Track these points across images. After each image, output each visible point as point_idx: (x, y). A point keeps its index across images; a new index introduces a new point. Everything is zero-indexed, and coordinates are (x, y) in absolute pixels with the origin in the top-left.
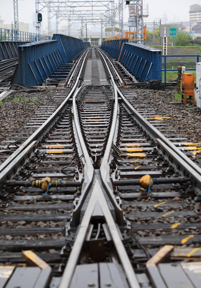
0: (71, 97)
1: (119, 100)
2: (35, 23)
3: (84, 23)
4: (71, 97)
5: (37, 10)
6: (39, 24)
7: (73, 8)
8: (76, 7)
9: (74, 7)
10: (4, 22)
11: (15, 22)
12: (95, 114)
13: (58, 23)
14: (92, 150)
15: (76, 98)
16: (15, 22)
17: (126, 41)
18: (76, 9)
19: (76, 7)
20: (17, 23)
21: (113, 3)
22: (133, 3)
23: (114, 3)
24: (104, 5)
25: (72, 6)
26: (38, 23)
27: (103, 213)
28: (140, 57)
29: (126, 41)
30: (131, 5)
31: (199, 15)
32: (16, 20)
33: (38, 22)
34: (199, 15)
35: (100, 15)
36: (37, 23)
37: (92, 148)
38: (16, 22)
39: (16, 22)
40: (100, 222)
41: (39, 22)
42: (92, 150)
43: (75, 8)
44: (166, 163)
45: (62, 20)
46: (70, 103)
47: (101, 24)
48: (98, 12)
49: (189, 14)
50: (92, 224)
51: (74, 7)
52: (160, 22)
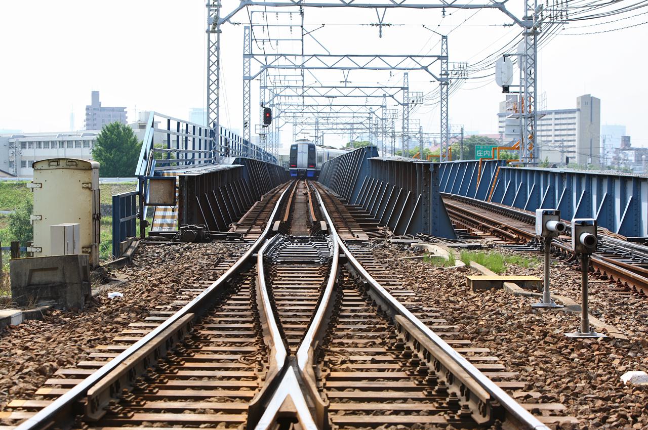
0: (256, 250)
1: (340, 259)
2: (258, 127)
3: (320, 130)
4: (256, 250)
5: (263, 102)
6: (264, 130)
7: (331, 99)
8: (336, 97)
9: (333, 97)
10: (159, 124)
11: (245, 124)
12: (289, 273)
13: (279, 128)
14: (285, 326)
15: (264, 253)
16: (245, 124)
17: (503, 164)
18: (335, 101)
19: (336, 97)
20: (248, 125)
21: (406, 91)
22: (519, 91)
23: (408, 92)
24: (390, 96)
25: (329, 94)
26: (263, 126)
27: (295, 408)
28: (406, 191)
29: (503, 164)
30: (511, 94)
31: (556, 119)
32: (247, 119)
33: (263, 124)
34: (556, 119)
35: (368, 115)
36: (261, 127)
37: (285, 323)
38: (247, 123)
39: (247, 123)
40: (293, 422)
41: (266, 125)
42: (285, 326)
43: (335, 99)
44: (400, 343)
45: (286, 123)
46: (252, 260)
47: (316, 130)
48: (346, 109)
49: (497, 119)
50: (278, 423)
51: (333, 97)
52: (462, 134)
